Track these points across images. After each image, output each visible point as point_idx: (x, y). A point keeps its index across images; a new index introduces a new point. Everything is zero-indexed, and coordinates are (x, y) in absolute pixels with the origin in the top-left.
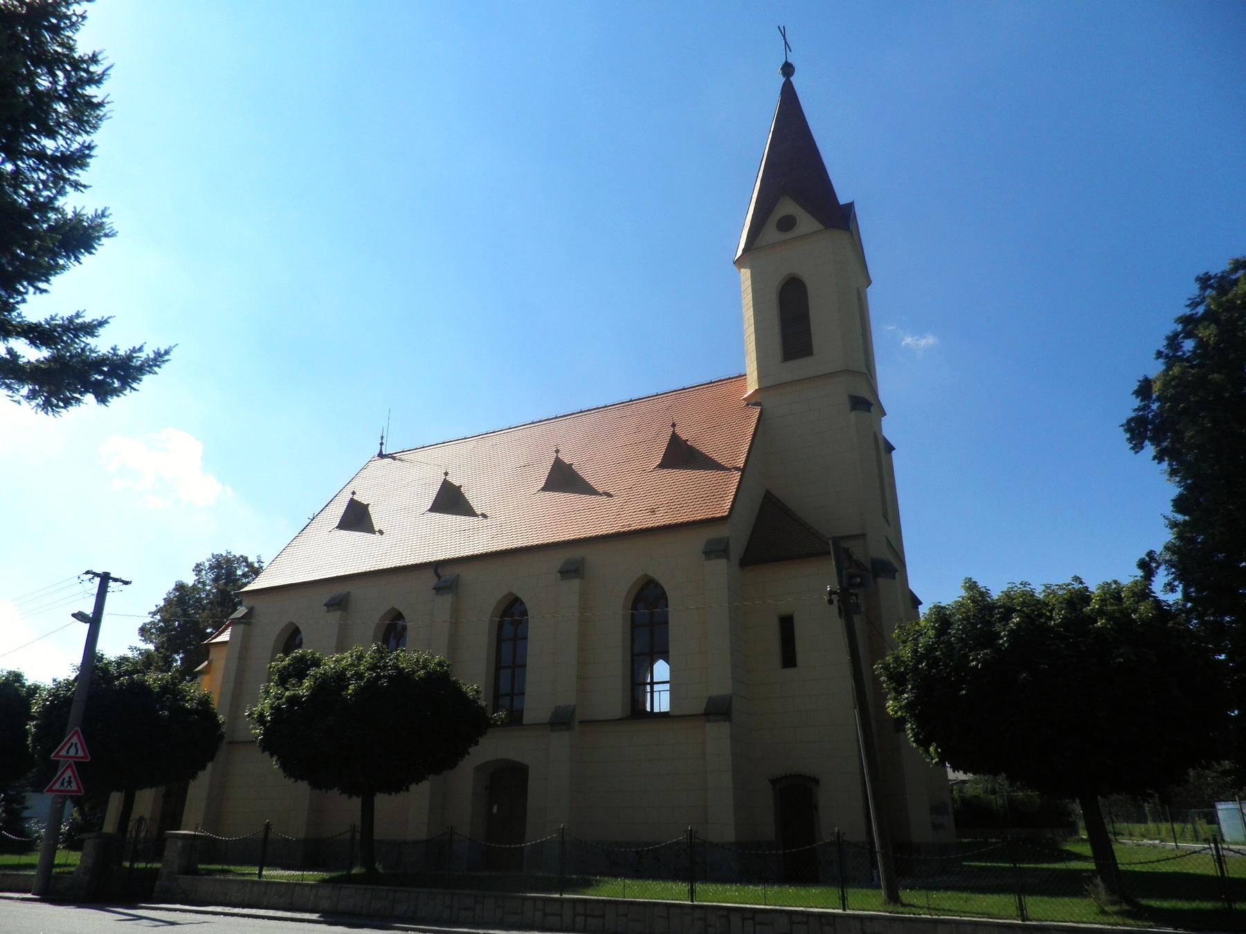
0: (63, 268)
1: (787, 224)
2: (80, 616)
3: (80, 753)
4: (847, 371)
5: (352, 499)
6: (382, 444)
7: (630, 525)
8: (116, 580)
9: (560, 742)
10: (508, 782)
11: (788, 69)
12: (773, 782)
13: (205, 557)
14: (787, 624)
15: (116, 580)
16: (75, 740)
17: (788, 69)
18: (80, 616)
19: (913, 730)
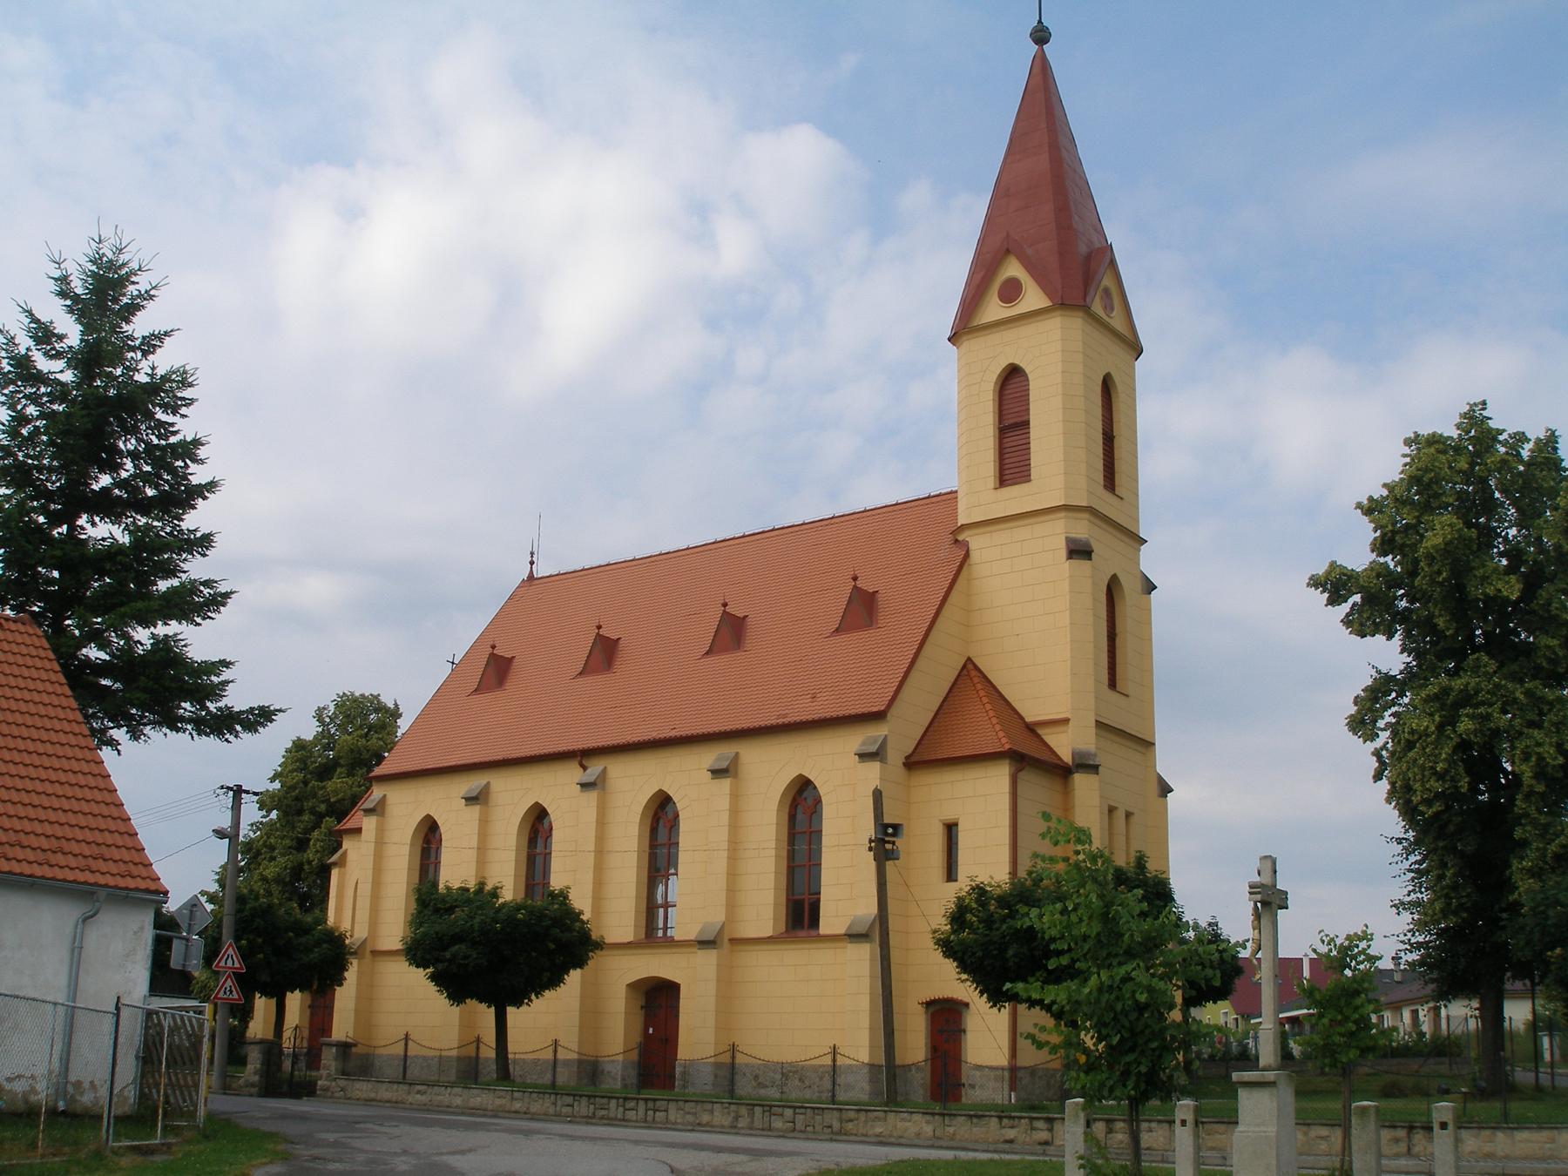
0: (272, 780)
1: (1011, 292)
2: (220, 834)
3: (237, 965)
4: (1066, 508)
5: (492, 655)
6: (532, 563)
7: (785, 716)
8: (247, 792)
9: (707, 962)
10: (659, 999)
11: (1041, 36)
12: (929, 1004)
13: (328, 699)
14: (951, 829)
15: (247, 792)
16: (231, 951)
17: (1041, 36)
18: (220, 834)
19: (466, 957)
